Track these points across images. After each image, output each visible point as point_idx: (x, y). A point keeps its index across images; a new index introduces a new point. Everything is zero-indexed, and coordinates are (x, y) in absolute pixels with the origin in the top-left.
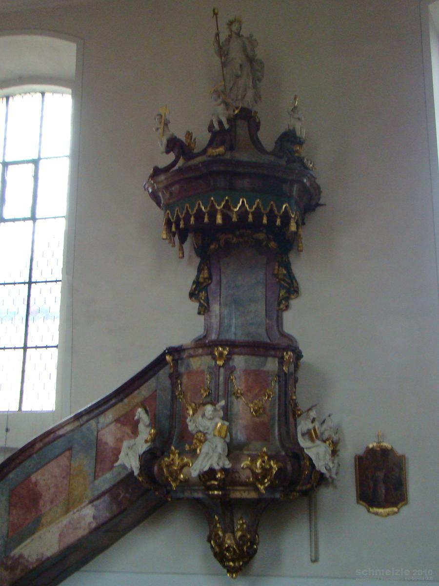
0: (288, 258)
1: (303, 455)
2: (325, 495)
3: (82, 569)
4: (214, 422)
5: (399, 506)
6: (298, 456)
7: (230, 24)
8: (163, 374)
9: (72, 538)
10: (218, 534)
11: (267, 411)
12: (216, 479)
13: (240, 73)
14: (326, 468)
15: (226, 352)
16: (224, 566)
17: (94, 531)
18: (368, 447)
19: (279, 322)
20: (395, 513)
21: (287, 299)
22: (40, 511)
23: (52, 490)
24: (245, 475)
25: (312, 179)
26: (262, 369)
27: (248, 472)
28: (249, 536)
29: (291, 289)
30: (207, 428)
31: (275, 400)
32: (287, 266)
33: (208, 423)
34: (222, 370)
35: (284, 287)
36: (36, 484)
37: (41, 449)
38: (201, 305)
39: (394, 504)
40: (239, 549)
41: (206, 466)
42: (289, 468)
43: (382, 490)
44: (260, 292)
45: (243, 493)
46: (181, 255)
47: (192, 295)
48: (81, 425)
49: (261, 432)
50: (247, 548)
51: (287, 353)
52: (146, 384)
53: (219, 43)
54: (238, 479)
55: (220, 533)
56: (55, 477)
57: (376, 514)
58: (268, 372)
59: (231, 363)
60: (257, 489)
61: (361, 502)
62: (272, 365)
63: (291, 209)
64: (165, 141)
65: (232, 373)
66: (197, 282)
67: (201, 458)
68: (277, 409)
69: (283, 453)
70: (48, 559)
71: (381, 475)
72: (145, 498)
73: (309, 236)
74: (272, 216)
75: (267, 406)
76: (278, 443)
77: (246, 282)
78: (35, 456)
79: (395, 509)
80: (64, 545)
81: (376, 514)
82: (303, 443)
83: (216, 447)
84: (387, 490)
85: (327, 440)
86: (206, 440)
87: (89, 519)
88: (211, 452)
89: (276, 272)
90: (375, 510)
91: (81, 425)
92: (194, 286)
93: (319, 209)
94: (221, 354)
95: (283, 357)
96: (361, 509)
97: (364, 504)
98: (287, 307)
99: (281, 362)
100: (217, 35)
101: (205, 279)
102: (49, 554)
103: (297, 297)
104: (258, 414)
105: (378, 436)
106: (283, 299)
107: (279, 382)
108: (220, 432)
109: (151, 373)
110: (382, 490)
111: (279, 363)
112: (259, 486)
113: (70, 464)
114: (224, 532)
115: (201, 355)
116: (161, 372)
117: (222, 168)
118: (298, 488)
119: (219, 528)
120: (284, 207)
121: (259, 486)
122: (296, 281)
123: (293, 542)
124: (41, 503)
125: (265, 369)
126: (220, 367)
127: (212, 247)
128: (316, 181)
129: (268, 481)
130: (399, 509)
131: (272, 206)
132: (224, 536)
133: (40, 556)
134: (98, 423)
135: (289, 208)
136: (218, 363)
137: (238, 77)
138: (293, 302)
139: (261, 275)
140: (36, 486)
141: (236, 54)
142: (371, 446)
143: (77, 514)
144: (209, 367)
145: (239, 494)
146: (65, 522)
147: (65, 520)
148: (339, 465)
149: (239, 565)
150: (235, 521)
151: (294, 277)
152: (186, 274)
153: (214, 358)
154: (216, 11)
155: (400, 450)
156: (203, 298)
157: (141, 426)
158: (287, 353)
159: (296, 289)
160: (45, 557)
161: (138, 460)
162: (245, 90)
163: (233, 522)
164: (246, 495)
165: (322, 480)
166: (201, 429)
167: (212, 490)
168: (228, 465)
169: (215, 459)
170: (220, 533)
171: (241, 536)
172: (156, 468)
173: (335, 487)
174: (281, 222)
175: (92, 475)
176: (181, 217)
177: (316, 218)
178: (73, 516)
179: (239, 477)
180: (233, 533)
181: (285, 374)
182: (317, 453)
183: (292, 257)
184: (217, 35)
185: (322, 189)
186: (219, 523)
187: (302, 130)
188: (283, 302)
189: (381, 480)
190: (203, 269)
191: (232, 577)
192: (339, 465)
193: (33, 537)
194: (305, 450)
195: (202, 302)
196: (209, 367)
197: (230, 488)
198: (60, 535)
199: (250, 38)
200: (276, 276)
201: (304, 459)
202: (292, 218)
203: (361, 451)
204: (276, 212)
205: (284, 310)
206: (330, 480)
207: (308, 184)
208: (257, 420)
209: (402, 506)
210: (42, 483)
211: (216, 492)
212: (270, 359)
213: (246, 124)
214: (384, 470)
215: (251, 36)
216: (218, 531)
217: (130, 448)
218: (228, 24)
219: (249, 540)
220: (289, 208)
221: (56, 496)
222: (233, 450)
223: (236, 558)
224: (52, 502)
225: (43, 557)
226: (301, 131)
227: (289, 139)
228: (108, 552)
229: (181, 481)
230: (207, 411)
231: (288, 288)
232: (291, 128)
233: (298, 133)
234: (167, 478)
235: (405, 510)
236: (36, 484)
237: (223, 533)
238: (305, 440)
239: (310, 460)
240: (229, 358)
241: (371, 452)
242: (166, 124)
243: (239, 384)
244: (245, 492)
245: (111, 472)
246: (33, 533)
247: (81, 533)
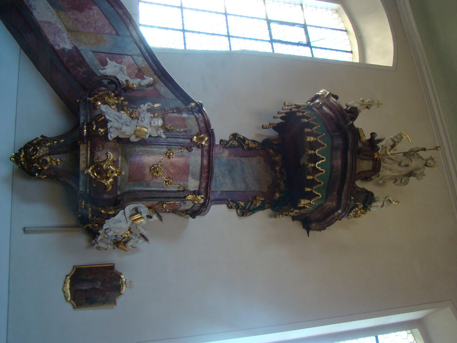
0: (268, 208)
1: (118, 208)
2: (81, 239)
3: (22, 51)
4: (148, 126)
5: (72, 302)
6: (117, 204)
7: (432, 159)
8: (179, 104)
9: (46, 30)
10: (47, 143)
11: (154, 180)
12: (97, 128)
13: (402, 164)
14: (108, 229)
15: (204, 143)
16: (20, 151)
17: (52, 47)
18: (121, 274)
19: (219, 201)
20: (66, 298)
21: (237, 207)
22: (70, 11)
23: (85, 20)
24: (100, 155)
25: (340, 218)
26: (190, 175)
27: (104, 158)
28: (46, 168)
29: (244, 212)
30: (143, 120)
31: (163, 187)
32: (261, 208)
33: (147, 121)
34: (189, 141)
35: (246, 205)
36: (91, 9)
37: (118, 13)
38: (228, 142)
39: (74, 298)
40: (35, 158)
41: (109, 116)
42: (106, 196)
43: (85, 287)
44: (241, 186)
45: (85, 156)
46: (265, 126)
47: (235, 136)
48: (136, 43)
49: (136, 175)
50: (36, 166)
51: (202, 198)
52: (169, 92)
53: (418, 151)
54: (97, 149)
55: (48, 144)
56: (96, 23)
57: (65, 283)
58: (187, 181)
59: (194, 148)
60: (88, 168)
61: (75, 269)
62: (193, 184)
63: (317, 200)
64: (356, 105)
65: (187, 149)
66: (244, 139)
67: (117, 113)
68: (156, 189)
69: (119, 193)
70: (31, 13)
71: (98, 285)
72: (78, 87)
73: (287, 224)
74: (312, 183)
75: (159, 180)
76: (127, 189)
77: (247, 175)
78: (112, 9)
79: (69, 299)
80: (41, 25)
81: (65, 283)
82: (129, 208)
83: (127, 125)
84: (85, 291)
85: (131, 232)
86: (133, 118)
87: (62, 46)
88: (122, 121)
89: (258, 198)
90: (68, 282)
91: (136, 43)
92: (242, 137)
93: (305, 231)
94: (202, 139)
95: (199, 194)
96: (68, 270)
97: (73, 272)
98: (230, 207)
99: (196, 193)
100: (424, 149)
101: (248, 145)
102: (35, 13)
103: (238, 215)
104: (152, 171)
105: (285, 103)
106: (237, 203)
107: (179, 191)
108: (140, 130)
109: (179, 95)
110: (85, 287)
111: (194, 191)
112: (91, 169)
113: (106, 34)
114: (50, 147)
115: (199, 125)
116: (180, 102)
117: (350, 141)
118: (89, 205)
119: (53, 143)
120: (319, 194)
121: (91, 169)
122: (251, 214)
123: (42, 213)
124: (76, 12)
125: (190, 178)
126: (191, 140)
127: (271, 151)
128: (338, 221)
129: (96, 177)
130: (70, 301)
131: (320, 183)
132: (46, 147)
133: (33, 7)
134: (138, 56)
135: (318, 198)
136: (195, 137)
137: (400, 164)
138: (234, 212)
139: (254, 187)
140: (89, 9)
141: (414, 164)
142: (122, 276)
143: (66, 36)
144: (190, 131)
145: (84, 153)
146: (60, 26)
147: (60, 26)
148: (106, 249)
149: (21, 162)
150: (59, 156)
151: (254, 213)
152: (251, 132)
153: (197, 135)
154: (439, 149)
155: (120, 300)
156: (233, 143)
157: (138, 80)
158: (202, 198)
159: (245, 214)
160: (33, 11)
161: (112, 74)
162: (390, 170)
163: (59, 153)
164: (82, 159)
165: (93, 234)
166: (142, 115)
167: (87, 127)
168: (111, 136)
169: (116, 125)
170: (48, 144)
171: (46, 162)
172: (104, 88)
173: (88, 247)
174: (308, 191)
175: (97, 50)
176: (305, 114)
177: (296, 228)
178: (65, 35)
179: (99, 150)
180: (49, 154)
181: (185, 197)
182: (118, 224)
183: (268, 211)
184: (424, 149)
185: (322, 231)
186: (57, 143)
187: (376, 208)
188: (234, 204)
189: (94, 286)
190: (254, 143)
191: (12, 157)
192: (106, 249)
193: (49, 5)
194: (122, 211)
195: (231, 142)
196: (190, 131)
197: (89, 144)
198: (50, 23)
199: (423, 174)
200: (255, 198)
201: (115, 209)
202: (311, 201)
203: (118, 268)
204: (315, 187)
205: (228, 206)
206: (93, 242)
207: (336, 214)
208: (147, 170)
209: (72, 304)
210: (91, 13)
211: (85, 130)
212: (198, 183)
213: (370, 169)
214: (102, 288)
215: (424, 175)
216: (51, 142)
217: (121, 69)
218: (431, 157)
219: (42, 169)
220: (318, 198)
221: (80, 23)
222: (123, 142)
223: (28, 162)
224: (76, 19)
225: (33, 9)
226: (375, 208)
227: (368, 199)
228: (36, 71)
229: (94, 104)
230: (157, 119)
231: (244, 206)
232: (376, 199)
233: (374, 204)
234: (97, 94)
235: (69, 306)
236: (91, 9)
237: (49, 146)
238: (131, 211)
239: (114, 215)
240: (200, 146)
241: (118, 277)
242: (367, 107)
243: (177, 159)
244: (85, 158)
245: (99, 64)
246: (51, 5)
247: (51, 38)
